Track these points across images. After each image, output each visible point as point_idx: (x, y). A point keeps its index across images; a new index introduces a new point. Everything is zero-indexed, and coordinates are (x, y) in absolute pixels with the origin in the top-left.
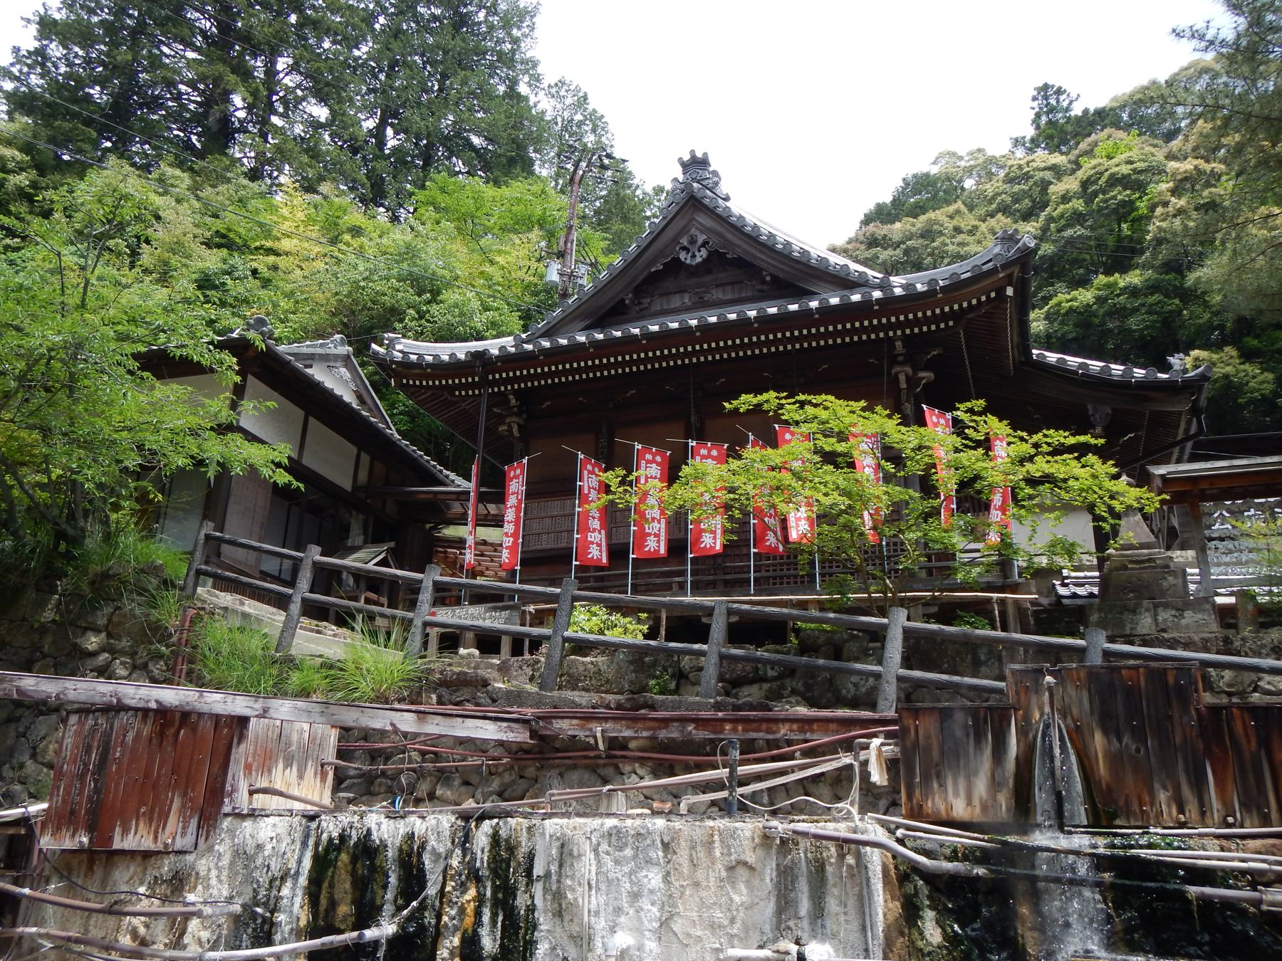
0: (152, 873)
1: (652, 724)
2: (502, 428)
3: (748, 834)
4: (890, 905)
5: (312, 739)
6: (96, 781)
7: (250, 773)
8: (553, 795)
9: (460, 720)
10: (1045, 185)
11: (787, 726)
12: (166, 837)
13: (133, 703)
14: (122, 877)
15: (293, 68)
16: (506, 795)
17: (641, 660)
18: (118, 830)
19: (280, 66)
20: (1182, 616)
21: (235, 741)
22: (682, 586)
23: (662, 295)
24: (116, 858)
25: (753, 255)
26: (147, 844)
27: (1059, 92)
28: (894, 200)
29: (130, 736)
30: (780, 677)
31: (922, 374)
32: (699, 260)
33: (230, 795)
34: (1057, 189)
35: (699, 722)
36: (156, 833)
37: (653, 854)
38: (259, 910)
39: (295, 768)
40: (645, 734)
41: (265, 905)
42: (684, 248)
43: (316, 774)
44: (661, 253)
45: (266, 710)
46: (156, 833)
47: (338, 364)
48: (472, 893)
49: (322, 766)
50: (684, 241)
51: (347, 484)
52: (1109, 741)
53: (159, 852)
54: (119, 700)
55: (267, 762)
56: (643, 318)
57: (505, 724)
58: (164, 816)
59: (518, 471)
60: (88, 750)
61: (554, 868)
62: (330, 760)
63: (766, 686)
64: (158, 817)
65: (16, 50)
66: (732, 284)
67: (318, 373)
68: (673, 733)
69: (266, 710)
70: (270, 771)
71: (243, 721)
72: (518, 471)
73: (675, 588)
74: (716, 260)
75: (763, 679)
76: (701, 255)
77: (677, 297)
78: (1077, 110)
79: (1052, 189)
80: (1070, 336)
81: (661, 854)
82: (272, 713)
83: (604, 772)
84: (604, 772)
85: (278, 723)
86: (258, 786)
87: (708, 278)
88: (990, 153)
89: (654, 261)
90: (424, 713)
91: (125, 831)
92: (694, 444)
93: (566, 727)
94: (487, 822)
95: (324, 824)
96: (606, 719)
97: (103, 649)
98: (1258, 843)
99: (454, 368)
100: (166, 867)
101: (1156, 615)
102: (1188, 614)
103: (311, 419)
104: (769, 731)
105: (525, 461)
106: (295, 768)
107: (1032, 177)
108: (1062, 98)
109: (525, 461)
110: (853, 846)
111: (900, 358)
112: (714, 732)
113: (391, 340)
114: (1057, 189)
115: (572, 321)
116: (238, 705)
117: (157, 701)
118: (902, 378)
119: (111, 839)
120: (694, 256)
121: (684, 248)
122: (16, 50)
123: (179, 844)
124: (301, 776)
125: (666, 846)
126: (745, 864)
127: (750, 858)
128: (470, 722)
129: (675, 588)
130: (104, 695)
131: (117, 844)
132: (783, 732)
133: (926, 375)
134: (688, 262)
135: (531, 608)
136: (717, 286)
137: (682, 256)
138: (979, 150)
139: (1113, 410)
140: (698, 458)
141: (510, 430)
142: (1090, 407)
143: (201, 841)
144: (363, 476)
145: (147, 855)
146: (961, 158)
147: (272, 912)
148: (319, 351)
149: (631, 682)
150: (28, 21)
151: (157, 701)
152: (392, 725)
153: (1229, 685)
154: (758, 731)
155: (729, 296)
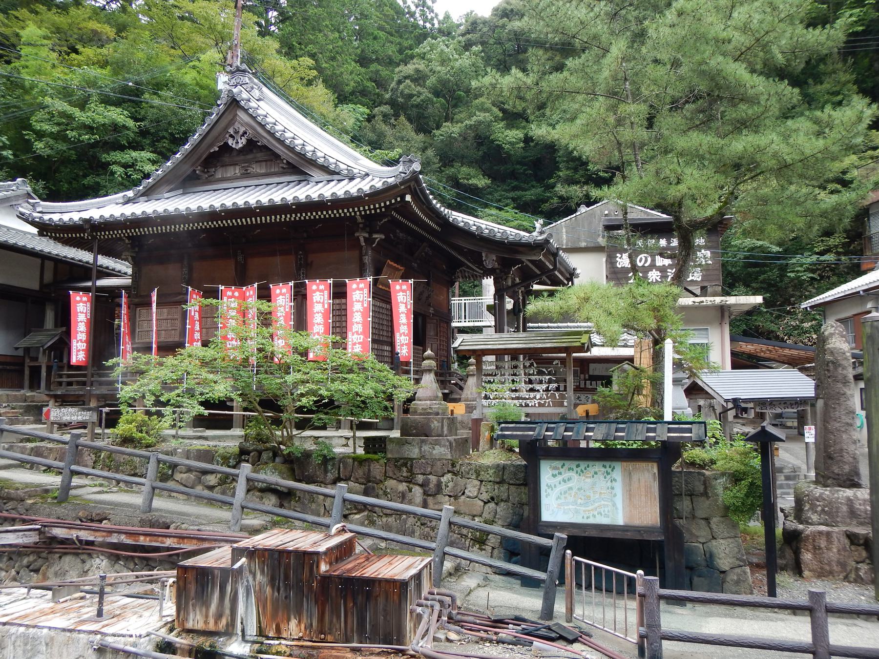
1: (104, 534)
23: (222, 166)
24: (260, 155)
25: (273, 145)
31: (375, 236)
32: (240, 145)
35: (128, 534)
42: (231, 136)
44: (216, 139)
47: (19, 202)
50: (231, 131)
51: (35, 285)
52: (273, 592)
66: (266, 161)
68: (114, 539)
74: (252, 145)
76: (242, 142)
77: (232, 168)
81: (44, 648)
87: (250, 156)
89: (211, 145)
92: (223, 288)
93: (60, 532)
111: (361, 226)
118: (362, 239)
120: (237, 143)
121: (231, 136)
133: (378, 237)
134: (234, 146)
135: (107, 409)
136: (256, 162)
137: (230, 142)
140: (225, 299)
142: (484, 255)
155: (263, 171)
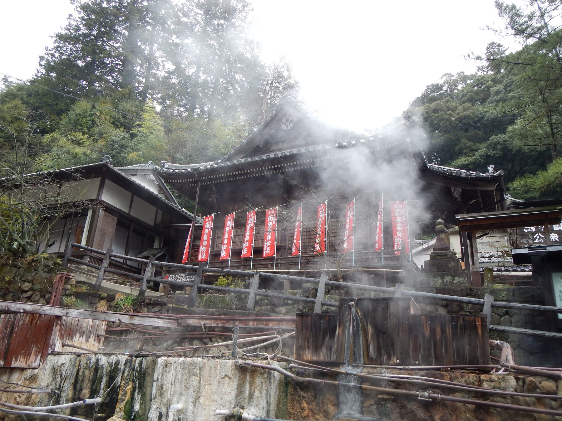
0: (24, 376)
2: (210, 199)
3: (230, 364)
4: (282, 394)
5: (93, 326)
6: (8, 340)
7: (63, 338)
8: (177, 349)
9: (148, 318)
10: (489, 87)
11: (273, 322)
12: (29, 362)
13: (14, 310)
14: (15, 378)
15: (158, 49)
16: (168, 349)
17: (240, 296)
18: (14, 359)
19: (154, 48)
20: (454, 279)
21: (55, 325)
22: (272, 265)
26: (23, 365)
27: (499, 46)
28: (422, 96)
29: (21, 323)
30: (293, 304)
33: (51, 346)
34: (493, 89)
36: (26, 361)
37: (195, 371)
38: (56, 391)
39: (84, 337)
40: (220, 325)
41: (59, 389)
43: (95, 340)
45: (67, 313)
46: (26, 361)
47: (149, 174)
48: (130, 386)
49: (98, 336)
53: (26, 369)
54: (8, 309)
55: (71, 334)
56: (268, 153)
57: (167, 320)
58: (29, 354)
59: (210, 219)
60: (6, 328)
61: (160, 377)
62: (102, 334)
63: (288, 307)
64: (27, 355)
65: (47, 48)
67: (137, 180)
69: (67, 313)
70: (72, 338)
71: (58, 317)
72: (210, 219)
73: (269, 266)
75: (287, 304)
78: (507, 53)
79: (491, 89)
80: (497, 155)
82: (70, 315)
83: (205, 341)
84: (205, 341)
85: (77, 319)
86: (66, 343)
88: (465, 74)
90: (133, 315)
91: (16, 360)
94: (139, 358)
95: (82, 358)
96: (206, 319)
97: (30, 289)
98: (425, 372)
99: (188, 175)
100: (29, 373)
101: (443, 278)
102: (456, 278)
103: (135, 197)
104: (266, 325)
105: (213, 215)
106: (84, 337)
107: (484, 84)
108: (500, 48)
109: (213, 215)
110: (267, 370)
112: (246, 325)
113: (164, 163)
114: (493, 89)
115: (238, 154)
116: (57, 311)
117: (23, 309)
119: (11, 363)
120: (287, 127)
122: (47, 48)
123: (34, 365)
124: (87, 340)
125: (200, 368)
126: (228, 376)
127: (230, 374)
128: (152, 319)
129: (269, 266)
130: (3, 306)
131: (13, 365)
132: (271, 325)
138: (462, 72)
139: (462, 190)
141: (213, 200)
142: (452, 189)
143: (41, 364)
144: (159, 220)
145: (23, 370)
146: (453, 76)
147: (61, 392)
148: (140, 168)
149: (236, 305)
150: (52, 37)
151: (23, 309)
152: (119, 320)
153: (470, 309)
154: (262, 324)
